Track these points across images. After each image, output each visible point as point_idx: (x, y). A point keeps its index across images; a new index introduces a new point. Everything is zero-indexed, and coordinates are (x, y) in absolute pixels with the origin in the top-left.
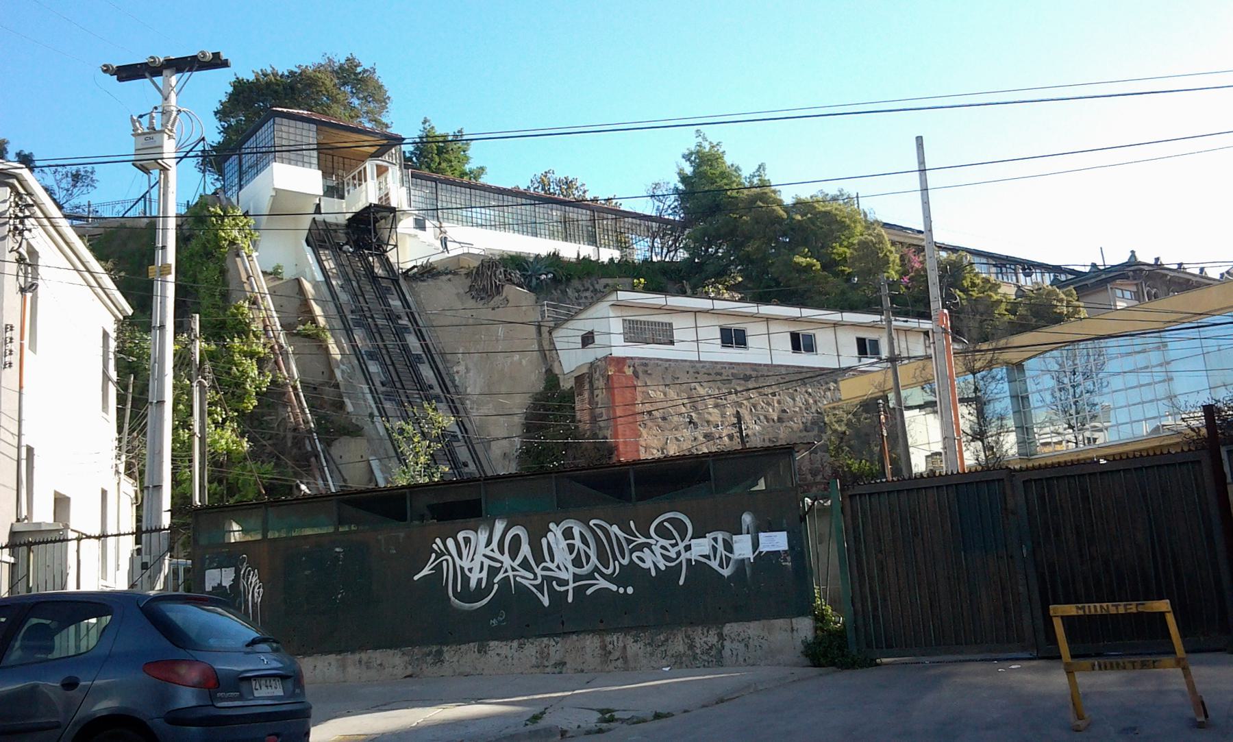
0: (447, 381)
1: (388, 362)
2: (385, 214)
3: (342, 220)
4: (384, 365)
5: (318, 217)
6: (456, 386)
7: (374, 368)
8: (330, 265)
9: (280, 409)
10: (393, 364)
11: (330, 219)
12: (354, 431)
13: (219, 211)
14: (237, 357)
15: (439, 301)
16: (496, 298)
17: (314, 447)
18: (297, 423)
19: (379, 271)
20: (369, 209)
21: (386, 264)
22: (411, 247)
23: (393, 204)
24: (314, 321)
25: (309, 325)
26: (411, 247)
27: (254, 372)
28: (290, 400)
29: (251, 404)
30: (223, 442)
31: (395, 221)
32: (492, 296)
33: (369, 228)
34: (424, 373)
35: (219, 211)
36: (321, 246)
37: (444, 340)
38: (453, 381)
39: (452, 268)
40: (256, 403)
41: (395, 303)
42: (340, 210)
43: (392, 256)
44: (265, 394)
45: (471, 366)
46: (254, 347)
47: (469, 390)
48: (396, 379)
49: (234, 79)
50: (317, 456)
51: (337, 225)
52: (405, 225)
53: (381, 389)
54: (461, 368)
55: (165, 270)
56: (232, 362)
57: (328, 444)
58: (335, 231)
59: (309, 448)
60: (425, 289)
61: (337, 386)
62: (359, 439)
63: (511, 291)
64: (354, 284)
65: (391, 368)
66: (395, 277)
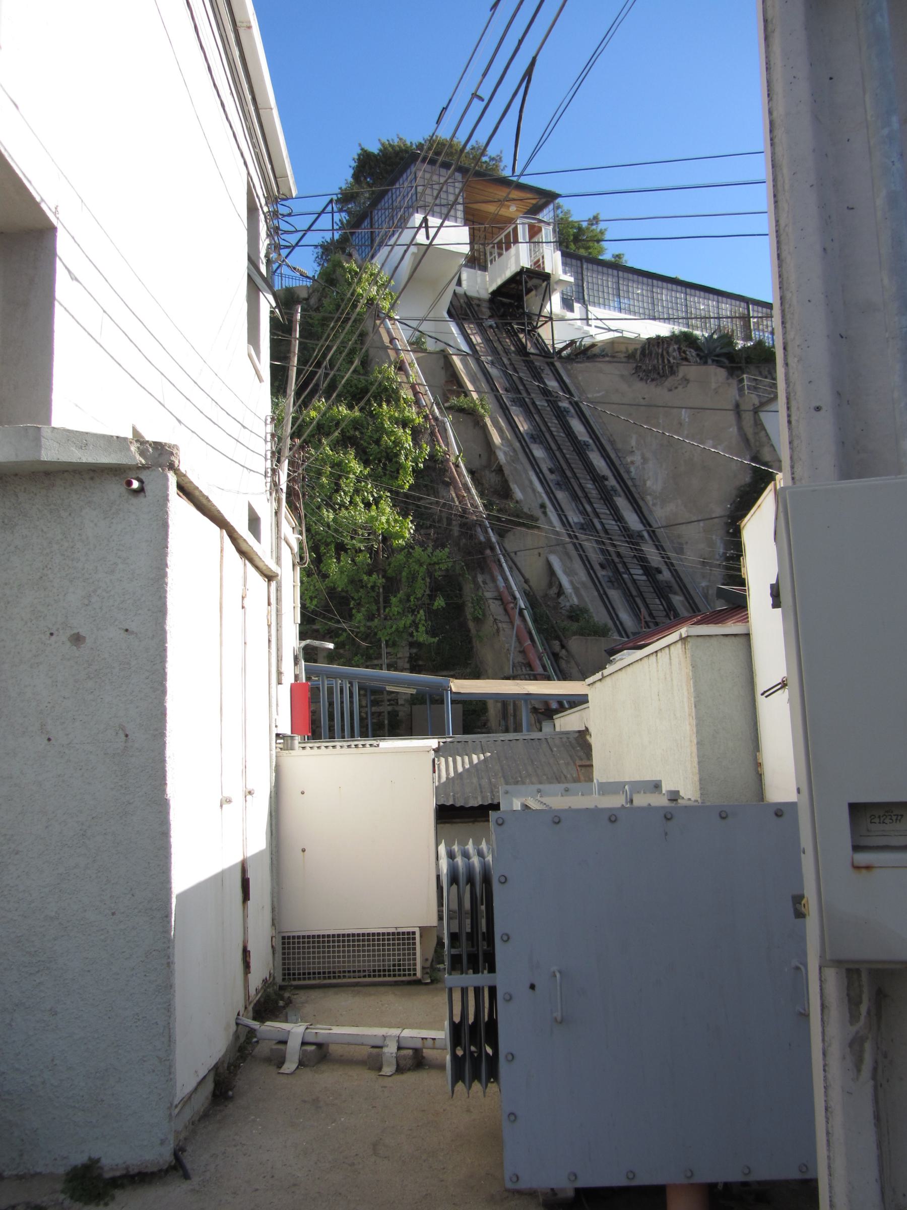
1: (554, 447)
2: (535, 281)
3: (485, 294)
4: (548, 449)
7: (539, 452)
8: (477, 339)
10: (560, 449)
12: (526, 521)
13: (355, 267)
14: (387, 424)
15: (598, 384)
16: (670, 379)
18: (465, 510)
19: (530, 348)
20: (522, 272)
21: (539, 343)
22: (566, 323)
24: (466, 394)
26: (566, 323)
27: (408, 443)
29: (407, 481)
30: (384, 519)
32: (664, 376)
33: (516, 301)
35: (355, 267)
40: (412, 481)
41: (552, 384)
42: (481, 284)
44: (421, 471)
46: (407, 414)
47: (649, 483)
48: (565, 466)
49: (360, 152)
50: (492, 549)
51: (479, 299)
52: (555, 304)
53: (550, 477)
54: (637, 458)
56: (380, 429)
57: (501, 534)
58: (478, 305)
59: (482, 538)
60: (583, 373)
61: (500, 470)
63: (691, 371)
66: (547, 355)
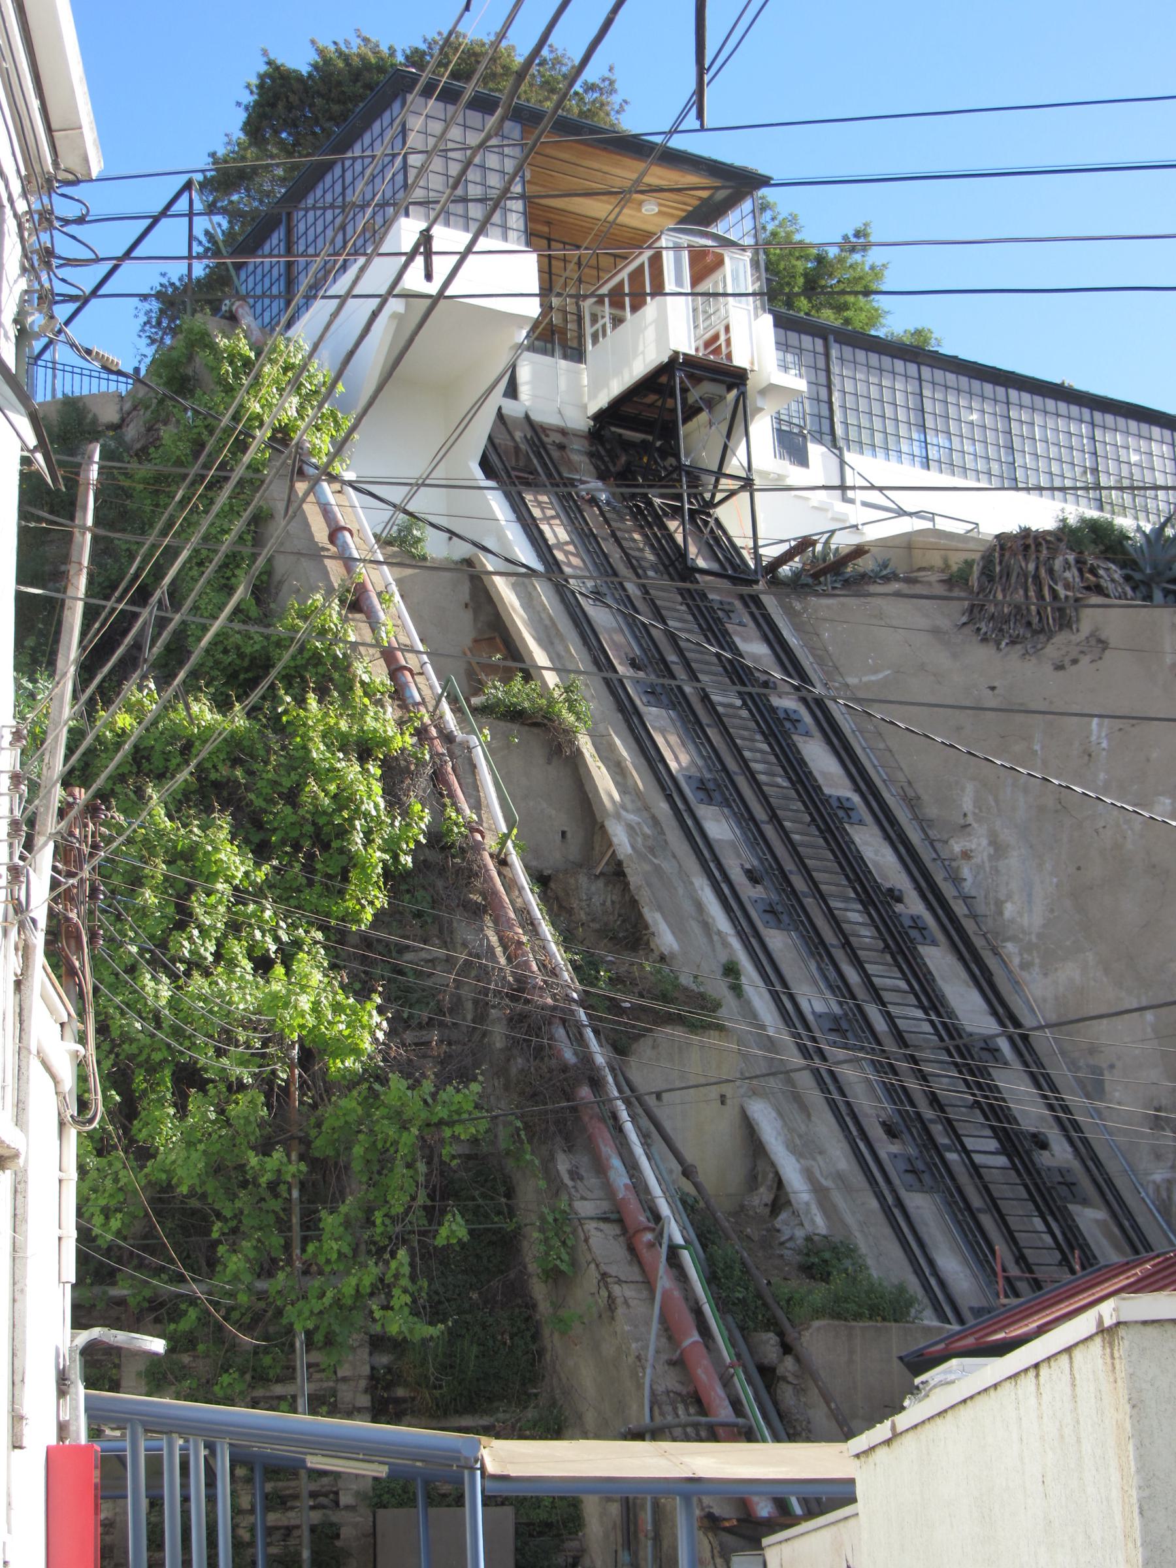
0: (939, 878)
4: (745, 819)
5: (512, 409)
6: (967, 899)
7: (719, 827)
9: (463, 930)
10: (774, 818)
11: (545, 415)
12: (693, 1012)
15: (871, 654)
16: (1060, 638)
17: (586, 1059)
21: (717, 542)
22: (781, 498)
23: (740, 360)
25: (517, 683)
26: (781, 498)
28: (490, 895)
29: (369, 902)
31: (738, 420)
33: (655, 438)
34: (868, 853)
36: (528, 484)
37: (910, 759)
38: (956, 880)
39: (899, 565)
40: (381, 901)
41: (754, 649)
42: (569, 394)
43: (732, 517)
44: (407, 874)
45: (1007, 835)
46: (370, 723)
47: (1009, 910)
50: (596, 1083)
51: (563, 432)
52: (758, 447)
53: (750, 892)
54: (978, 842)
55: (84, 528)
56: (301, 764)
57: (620, 1047)
59: (569, 1056)
61: (617, 873)
62: (712, 1039)
64: (631, 588)
65: (769, 831)
